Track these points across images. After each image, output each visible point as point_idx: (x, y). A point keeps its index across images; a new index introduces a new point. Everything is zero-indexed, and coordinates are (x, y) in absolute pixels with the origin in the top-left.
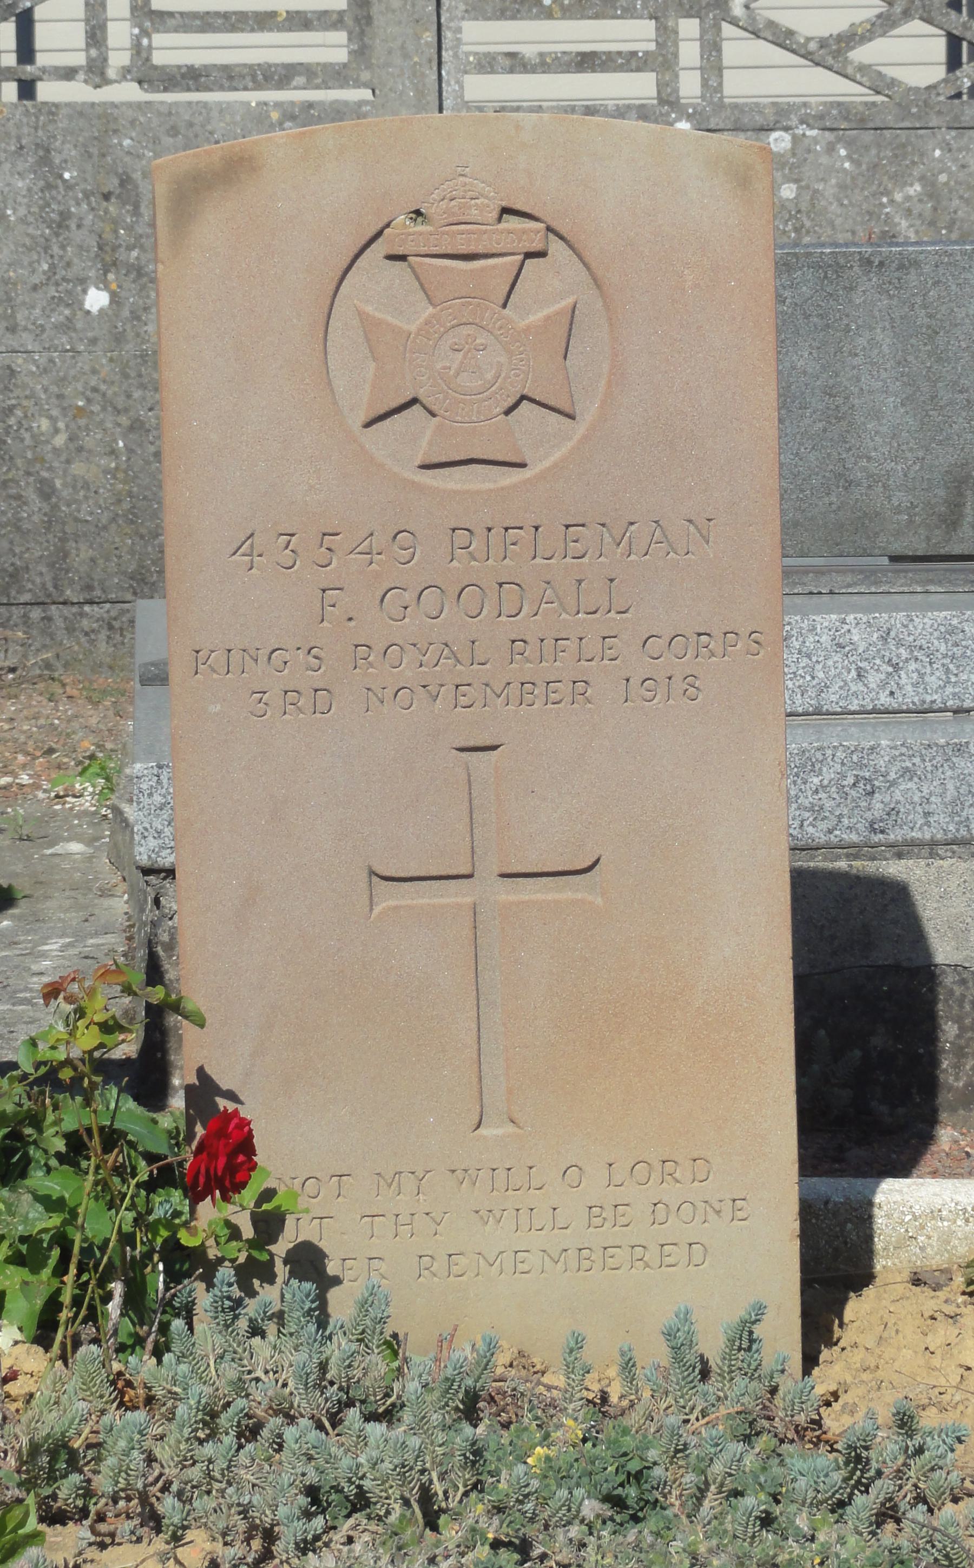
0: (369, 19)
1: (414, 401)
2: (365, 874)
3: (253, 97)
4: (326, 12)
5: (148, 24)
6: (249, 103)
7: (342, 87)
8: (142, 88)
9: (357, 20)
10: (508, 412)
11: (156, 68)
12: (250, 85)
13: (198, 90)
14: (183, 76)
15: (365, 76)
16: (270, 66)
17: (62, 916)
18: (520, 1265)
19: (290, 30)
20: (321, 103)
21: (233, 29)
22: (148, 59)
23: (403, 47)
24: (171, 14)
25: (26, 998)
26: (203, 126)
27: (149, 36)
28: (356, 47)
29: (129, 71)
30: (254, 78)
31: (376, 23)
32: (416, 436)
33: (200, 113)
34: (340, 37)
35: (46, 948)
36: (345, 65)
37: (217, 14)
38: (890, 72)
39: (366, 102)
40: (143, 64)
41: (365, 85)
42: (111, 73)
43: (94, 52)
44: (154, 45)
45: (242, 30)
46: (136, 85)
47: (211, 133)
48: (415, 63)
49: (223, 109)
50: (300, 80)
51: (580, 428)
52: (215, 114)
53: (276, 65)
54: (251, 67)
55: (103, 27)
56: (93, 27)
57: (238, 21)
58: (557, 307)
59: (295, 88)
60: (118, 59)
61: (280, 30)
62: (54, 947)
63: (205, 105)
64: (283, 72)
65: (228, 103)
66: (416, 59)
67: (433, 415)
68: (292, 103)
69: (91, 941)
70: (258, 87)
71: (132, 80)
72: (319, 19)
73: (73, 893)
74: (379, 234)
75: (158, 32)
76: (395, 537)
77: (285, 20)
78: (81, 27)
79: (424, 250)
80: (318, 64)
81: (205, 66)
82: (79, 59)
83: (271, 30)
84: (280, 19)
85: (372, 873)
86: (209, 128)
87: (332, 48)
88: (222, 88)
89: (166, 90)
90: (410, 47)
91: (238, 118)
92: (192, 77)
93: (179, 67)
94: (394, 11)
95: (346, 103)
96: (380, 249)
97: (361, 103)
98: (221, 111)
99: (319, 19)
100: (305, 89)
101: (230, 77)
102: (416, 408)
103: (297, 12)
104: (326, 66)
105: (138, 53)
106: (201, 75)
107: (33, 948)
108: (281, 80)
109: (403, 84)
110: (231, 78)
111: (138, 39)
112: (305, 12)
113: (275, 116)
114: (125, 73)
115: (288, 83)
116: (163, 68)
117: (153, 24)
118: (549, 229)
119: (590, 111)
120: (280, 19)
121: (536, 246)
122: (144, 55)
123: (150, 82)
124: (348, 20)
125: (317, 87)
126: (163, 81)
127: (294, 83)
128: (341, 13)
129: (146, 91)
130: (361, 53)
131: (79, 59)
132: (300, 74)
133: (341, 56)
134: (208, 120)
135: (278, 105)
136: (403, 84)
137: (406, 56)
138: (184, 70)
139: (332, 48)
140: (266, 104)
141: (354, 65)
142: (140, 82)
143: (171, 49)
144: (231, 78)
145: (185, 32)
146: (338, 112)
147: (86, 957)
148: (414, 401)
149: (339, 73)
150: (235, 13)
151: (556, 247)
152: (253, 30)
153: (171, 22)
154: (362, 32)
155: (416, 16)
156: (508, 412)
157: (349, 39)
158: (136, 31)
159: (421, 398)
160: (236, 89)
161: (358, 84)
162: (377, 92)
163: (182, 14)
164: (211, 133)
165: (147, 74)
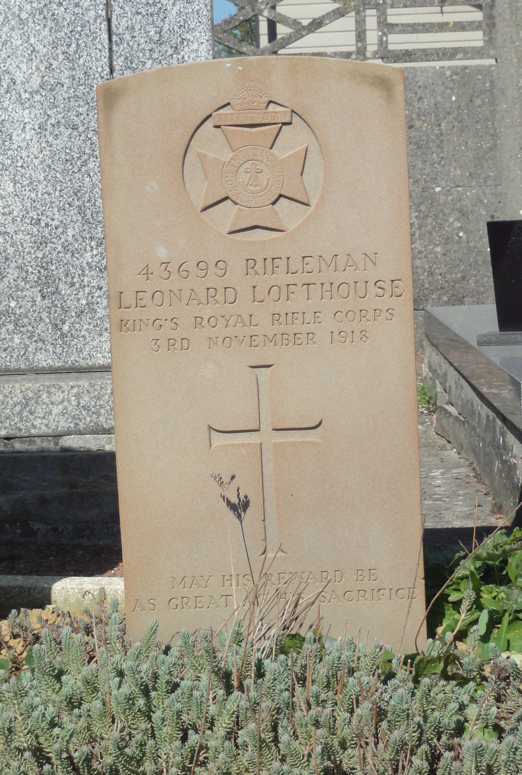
0: (494, 25)
1: (227, 198)
2: (206, 428)
3: (438, 64)
4: (472, 22)
5: (386, 30)
6: (435, 67)
7: (481, 58)
8: (383, 61)
9: (488, 25)
10: (274, 203)
11: (390, 51)
12: (436, 58)
13: (410, 61)
14: (403, 55)
15: (492, 52)
16: (445, 49)
17: (427, 459)
18: (198, 604)
19: (455, 31)
20: (471, 67)
21: (427, 31)
22: (386, 47)
23: (511, 38)
24: (397, 25)
25: (438, 498)
26: (413, 79)
27: (387, 36)
28: (487, 39)
29: (377, 53)
30: (438, 54)
31: (498, 27)
32: (226, 216)
33: (412, 73)
34: (479, 34)
35: (433, 474)
36: (482, 48)
37: (419, 24)
38: (300, 21)
39: (493, 66)
40: (384, 50)
41: (492, 57)
42: (368, 54)
43: (360, 44)
44: (389, 42)
45: (432, 32)
46: (381, 60)
47: (417, 82)
48: (517, 46)
49: (423, 70)
50: (460, 55)
51: (311, 209)
52: (419, 73)
53: (449, 48)
54: (436, 49)
55: (364, 32)
56: (359, 32)
57: (430, 27)
58: (297, 149)
59: (458, 59)
60: (371, 49)
61: (450, 31)
62: (437, 474)
63: (414, 68)
64: (452, 52)
65: (425, 67)
66: (517, 44)
67: (236, 204)
68: (457, 67)
69: (454, 471)
70: (440, 59)
71: (378, 58)
72: (469, 25)
73: (426, 449)
74: (210, 116)
75: (391, 34)
76: (216, 265)
77: (453, 26)
78: (354, 34)
79: (227, 123)
80: (469, 47)
81: (414, 50)
82: (353, 49)
83: (446, 31)
84: (450, 26)
85: (210, 428)
86: (416, 80)
87: (475, 39)
88: (422, 60)
89: (395, 62)
90: (515, 38)
91: (430, 75)
92: (408, 55)
93: (401, 50)
94: (506, 21)
95: (483, 66)
96: (209, 124)
97: (490, 66)
98: (422, 71)
99: (469, 25)
100: (462, 59)
101: (426, 55)
102: (228, 202)
103: (458, 22)
104: (473, 48)
105: (381, 44)
106: (412, 54)
107: (426, 474)
108: (451, 56)
109: (511, 56)
110: (426, 55)
111: (381, 37)
112: (462, 22)
113: (448, 73)
114: (375, 55)
115: (455, 57)
116: (394, 51)
117: (388, 30)
118: (293, 111)
119: (319, 54)
120: (450, 26)
121: (287, 120)
122: (384, 45)
123: (387, 58)
124: (484, 26)
125: (469, 59)
126: (393, 58)
127: (457, 57)
128: (480, 22)
129: (385, 63)
130: (490, 41)
131: (353, 49)
132: (460, 53)
133: (481, 44)
134: (415, 76)
135: (449, 68)
136: (511, 56)
137: (513, 42)
138: (403, 52)
139: (475, 39)
140: (444, 67)
141: (487, 48)
142: (382, 58)
143: (397, 42)
144: (426, 55)
145: (404, 33)
146: (479, 70)
147: (456, 479)
148: (227, 198)
149: (479, 52)
150: (428, 23)
151: (296, 119)
152: (437, 32)
153: (398, 29)
154: (491, 31)
155: (517, 23)
156: (274, 203)
157: (484, 35)
158: (380, 33)
159: (230, 196)
160: (429, 61)
161: (489, 57)
162: (498, 60)
163: (402, 25)
164: (417, 82)
165: (386, 55)
